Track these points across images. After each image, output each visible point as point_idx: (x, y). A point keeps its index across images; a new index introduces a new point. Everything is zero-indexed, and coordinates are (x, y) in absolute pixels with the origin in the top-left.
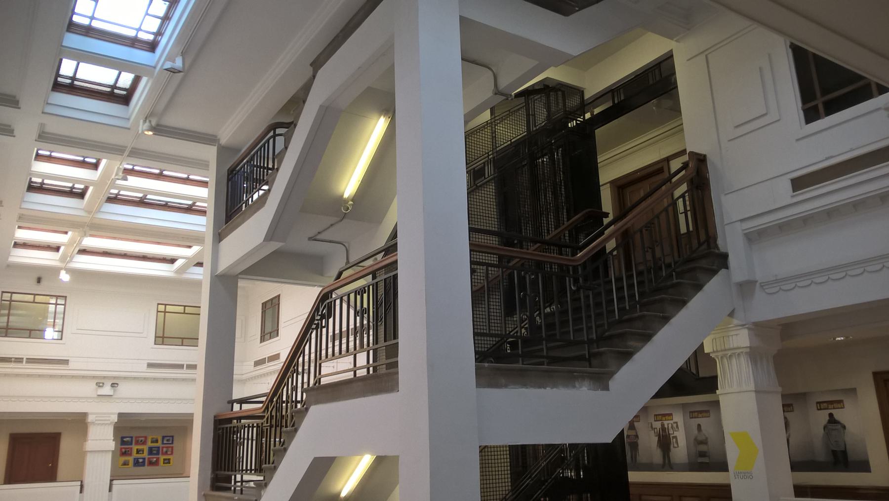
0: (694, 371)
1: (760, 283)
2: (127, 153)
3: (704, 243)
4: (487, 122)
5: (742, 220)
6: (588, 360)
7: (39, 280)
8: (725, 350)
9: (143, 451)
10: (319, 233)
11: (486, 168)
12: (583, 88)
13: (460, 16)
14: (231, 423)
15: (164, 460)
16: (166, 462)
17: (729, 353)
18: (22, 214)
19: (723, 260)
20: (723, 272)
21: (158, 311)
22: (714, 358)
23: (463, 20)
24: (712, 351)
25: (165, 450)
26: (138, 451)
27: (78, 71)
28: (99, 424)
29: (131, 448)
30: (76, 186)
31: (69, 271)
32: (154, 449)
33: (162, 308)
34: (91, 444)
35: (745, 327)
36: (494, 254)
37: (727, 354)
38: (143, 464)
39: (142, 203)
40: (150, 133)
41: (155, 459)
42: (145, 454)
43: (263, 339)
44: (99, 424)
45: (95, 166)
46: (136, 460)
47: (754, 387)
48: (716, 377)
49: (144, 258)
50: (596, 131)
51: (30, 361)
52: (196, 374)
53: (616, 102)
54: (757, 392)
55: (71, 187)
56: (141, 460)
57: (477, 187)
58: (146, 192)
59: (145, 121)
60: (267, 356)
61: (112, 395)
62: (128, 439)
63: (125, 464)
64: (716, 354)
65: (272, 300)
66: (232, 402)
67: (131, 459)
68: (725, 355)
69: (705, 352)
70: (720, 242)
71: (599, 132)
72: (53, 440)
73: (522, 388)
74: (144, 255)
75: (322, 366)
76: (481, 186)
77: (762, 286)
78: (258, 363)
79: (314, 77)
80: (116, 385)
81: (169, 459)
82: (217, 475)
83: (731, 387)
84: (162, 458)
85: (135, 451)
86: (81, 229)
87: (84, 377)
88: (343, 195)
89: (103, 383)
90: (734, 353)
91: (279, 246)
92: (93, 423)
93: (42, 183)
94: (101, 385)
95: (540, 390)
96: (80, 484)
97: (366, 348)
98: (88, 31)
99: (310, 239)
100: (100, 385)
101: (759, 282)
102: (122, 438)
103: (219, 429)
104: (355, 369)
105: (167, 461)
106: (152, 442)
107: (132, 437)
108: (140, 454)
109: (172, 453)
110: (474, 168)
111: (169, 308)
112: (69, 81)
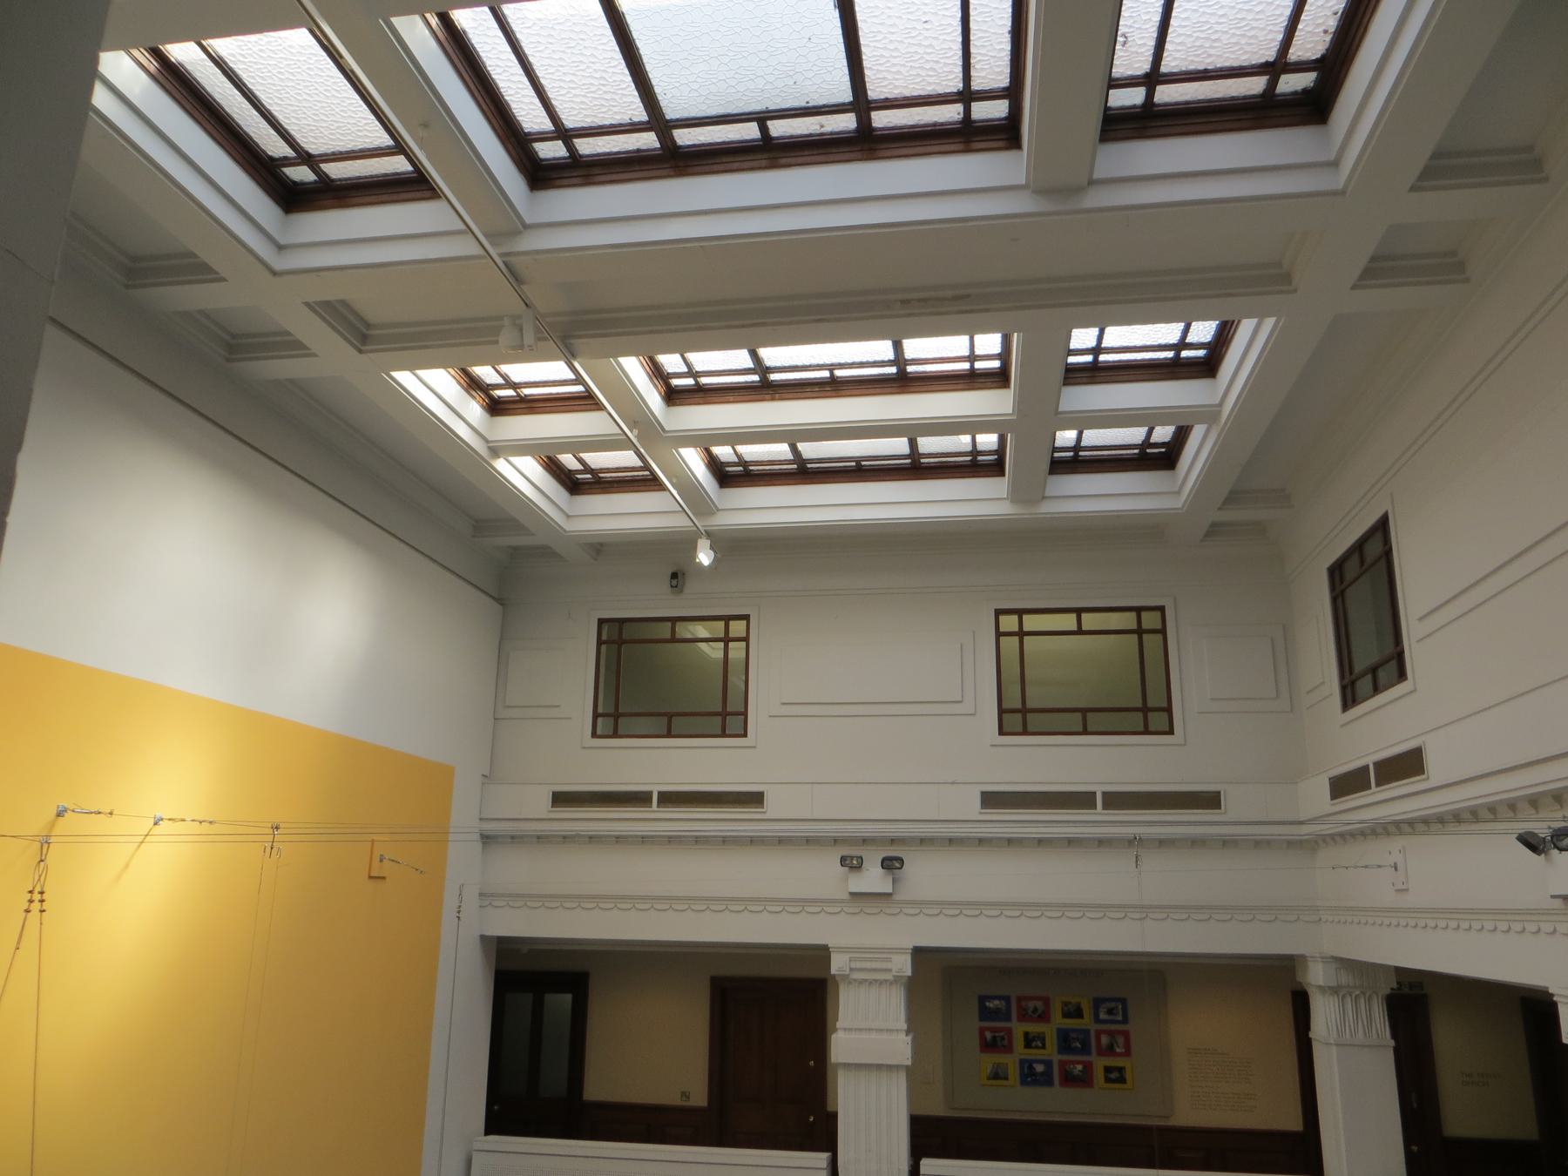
9: (1043, 1040)
15: (1108, 1070)
16: (1113, 1076)
21: (999, 634)
25: (1105, 1040)
26: (1029, 1041)
27: (1425, 612)
28: (861, 982)
29: (1009, 1031)
32: (1074, 1035)
33: (1009, 623)
34: (843, 1045)
38: (1045, 1079)
41: (1080, 1067)
42: (1051, 1051)
43: (1350, 699)
44: (861, 982)
46: (1026, 1065)
51: (668, 799)
56: (1039, 1068)
60: (1369, 760)
61: (889, 895)
62: (997, 1002)
63: (998, 1075)
65: (1359, 546)
67: (1011, 1062)
78: (1346, 785)
80: (898, 865)
81: (1121, 1070)
84: (1100, 1063)
85: (1019, 1042)
87: (810, 841)
100: (852, 864)
102: (982, 999)
105: (1116, 1076)
106: (1066, 1015)
107: (1007, 999)
108: (1037, 1047)
109: (1127, 1053)
111: (1031, 623)
112: (1089, 358)
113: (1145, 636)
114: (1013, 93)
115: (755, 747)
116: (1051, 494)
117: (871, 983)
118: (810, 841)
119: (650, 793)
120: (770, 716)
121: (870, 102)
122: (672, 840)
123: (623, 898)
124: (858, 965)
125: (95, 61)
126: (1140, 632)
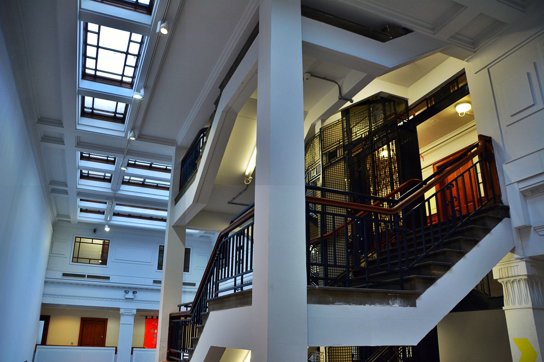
0: (487, 292)
1: (534, 228)
2: (125, 153)
3: (491, 199)
4: (339, 120)
5: (518, 182)
6: (401, 284)
7: (95, 231)
8: (509, 277)
10: (234, 199)
11: (338, 151)
12: (406, 98)
13: (303, 42)
14: (180, 319)
17: (512, 279)
18: (80, 192)
19: (505, 212)
20: (506, 219)
22: (500, 283)
23: (305, 45)
24: (499, 278)
28: (126, 315)
30: (107, 175)
31: (110, 226)
35: (523, 260)
36: (343, 208)
37: (511, 280)
39: (143, 185)
40: (133, 139)
44: (126, 315)
45: (113, 162)
47: (531, 305)
48: (503, 297)
49: (151, 218)
50: (418, 127)
51: (89, 277)
52: (161, 286)
53: (429, 106)
54: (533, 308)
55: (143, 181)
57: (332, 164)
58: (145, 177)
59: (131, 132)
61: (133, 298)
64: (502, 280)
66: (180, 306)
68: (509, 281)
69: (494, 279)
70: (503, 198)
71: (420, 128)
72: (104, 322)
73: (346, 304)
74: (151, 216)
75: (219, 285)
76: (334, 163)
77: (536, 230)
79: (221, 95)
80: (136, 293)
82: (170, 351)
83: (514, 305)
86: (110, 200)
87: (118, 287)
88: (245, 173)
89: (128, 291)
90: (515, 280)
91: (204, 206)
92: (123, 314)
93: (88, 174)
94: (127, 292)
95: (360, 306)
96: (115, 349)
97: (234, 276)
98: (95, 78)
99: (229, 203)
101: (533, 227)
103: (172, 322)
104: (242, 285)
110: (329, 151)
113: (77, 259)
114: (125, 114)
115: (116, 348)
116: (113, 220)
117: (128, 315)
118: (118, 287)
119: (85, 275)
120: (112, 262)
121: (85, 107)
122: (89, 285)
123: (76, 296)
124: (126, 312)
125: (320, 191)
126: (78, 258)
